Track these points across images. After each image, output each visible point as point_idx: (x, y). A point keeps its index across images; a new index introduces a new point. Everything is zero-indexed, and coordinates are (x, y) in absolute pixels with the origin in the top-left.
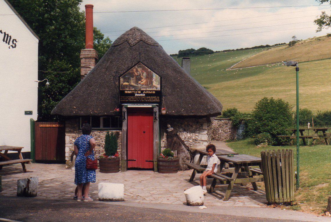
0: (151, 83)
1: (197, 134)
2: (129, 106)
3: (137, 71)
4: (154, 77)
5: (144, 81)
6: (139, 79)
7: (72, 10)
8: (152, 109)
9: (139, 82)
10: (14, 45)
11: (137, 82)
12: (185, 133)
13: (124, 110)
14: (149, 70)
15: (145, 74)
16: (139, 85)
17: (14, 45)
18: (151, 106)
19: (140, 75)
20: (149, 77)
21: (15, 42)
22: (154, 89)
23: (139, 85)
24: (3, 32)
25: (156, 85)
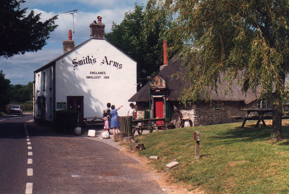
0: (162, 84)
1: (189, 111)
2: (153, 97)
3: (156, 78)
4: (163, 81)
5: (159, 84)
6: (157, 83)
7: (12, 3)
8: (162, 98)
9: (158, 84)
10: (120, 67)
11: (156, 85)
12: (184, 110)
13: (152, 98)
14: (161, 78)
15: (159, 80)
16: (158, 86)
17: (120, 67)
18: (161, 97)
19: (158, 80)
20: (161, 81)
21: (121, 66)
22: (163, 87)
23: (158, 86)
24: (113, 61)
25: (164, 86)
